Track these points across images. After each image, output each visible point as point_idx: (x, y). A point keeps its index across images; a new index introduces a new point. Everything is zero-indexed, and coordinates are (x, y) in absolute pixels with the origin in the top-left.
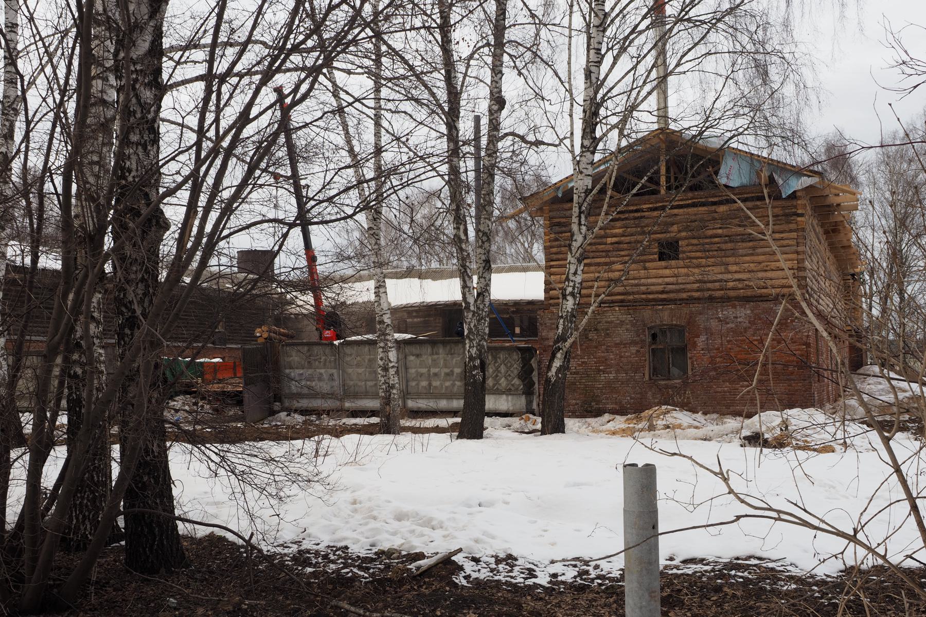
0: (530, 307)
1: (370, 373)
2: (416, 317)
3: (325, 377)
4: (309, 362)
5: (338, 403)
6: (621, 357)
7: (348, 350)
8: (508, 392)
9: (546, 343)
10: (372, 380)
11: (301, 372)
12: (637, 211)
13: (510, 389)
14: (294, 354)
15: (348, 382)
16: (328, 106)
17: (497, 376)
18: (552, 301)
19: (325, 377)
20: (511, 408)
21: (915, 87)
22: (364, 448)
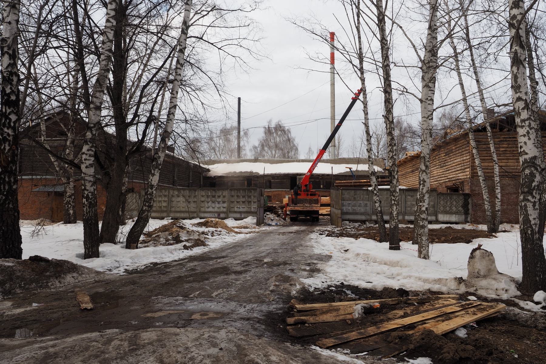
0: (327, 177)
1: (387, 203)
2: (276, 179)
4: (354, 198)
6: (509, 199)
8: (456, 213)
9: (474, 192)
11: (350, 202)
12: (513, 138)
13: (457, 212)
14: (346, 194)
17: (451, 206)
18: (475, 174)
20: (457, 220)
21: (316, 120)
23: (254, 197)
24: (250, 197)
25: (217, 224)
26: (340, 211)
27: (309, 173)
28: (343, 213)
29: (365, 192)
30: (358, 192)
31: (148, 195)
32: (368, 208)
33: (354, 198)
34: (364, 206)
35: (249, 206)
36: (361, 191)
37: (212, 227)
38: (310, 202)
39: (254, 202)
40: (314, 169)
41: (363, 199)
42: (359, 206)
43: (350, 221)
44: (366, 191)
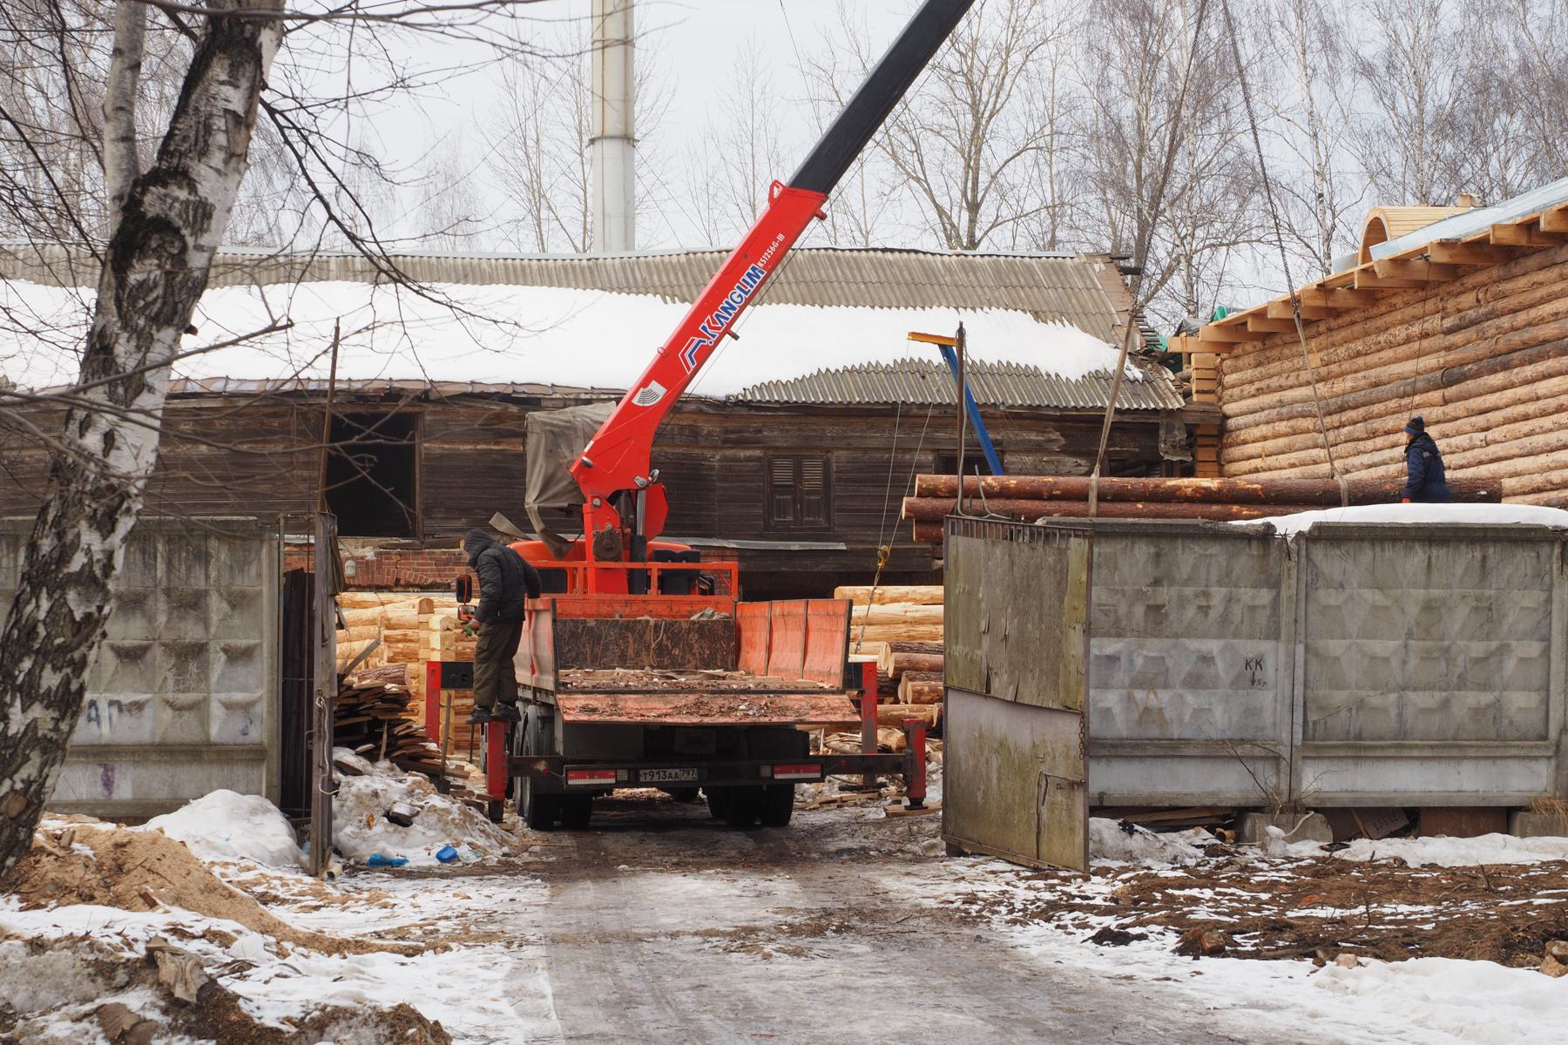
1: (1427, 657)
3: (1222, 669)
4: (1155, 610)
5: (1269, 778)
7: (1329, 562)
10: (1429, 687)
15: (1322, 692)
16: (89, 64)
19: (1222, 669)
22: (1255, 69)
23: (239, 601)
24: (192, 604)
25: (119, 869)
26: (1069, 729)
27: (658, 390)
28: (1093, 748)
29: (1246, 561)
30: (1186, 557)
31: (63, 586)
32: (1266, 698)
33: (1155, 610)
34: (1235, 683)
35: (181, 686)
36: (1215, 549)
37: (89, 899)
38: (661, 650)
39: (238, 656)
40: (704, 354)
41: (1225, 619)
42: (1195, 682)
43: (1131, 814)
44: (1255, 549)
